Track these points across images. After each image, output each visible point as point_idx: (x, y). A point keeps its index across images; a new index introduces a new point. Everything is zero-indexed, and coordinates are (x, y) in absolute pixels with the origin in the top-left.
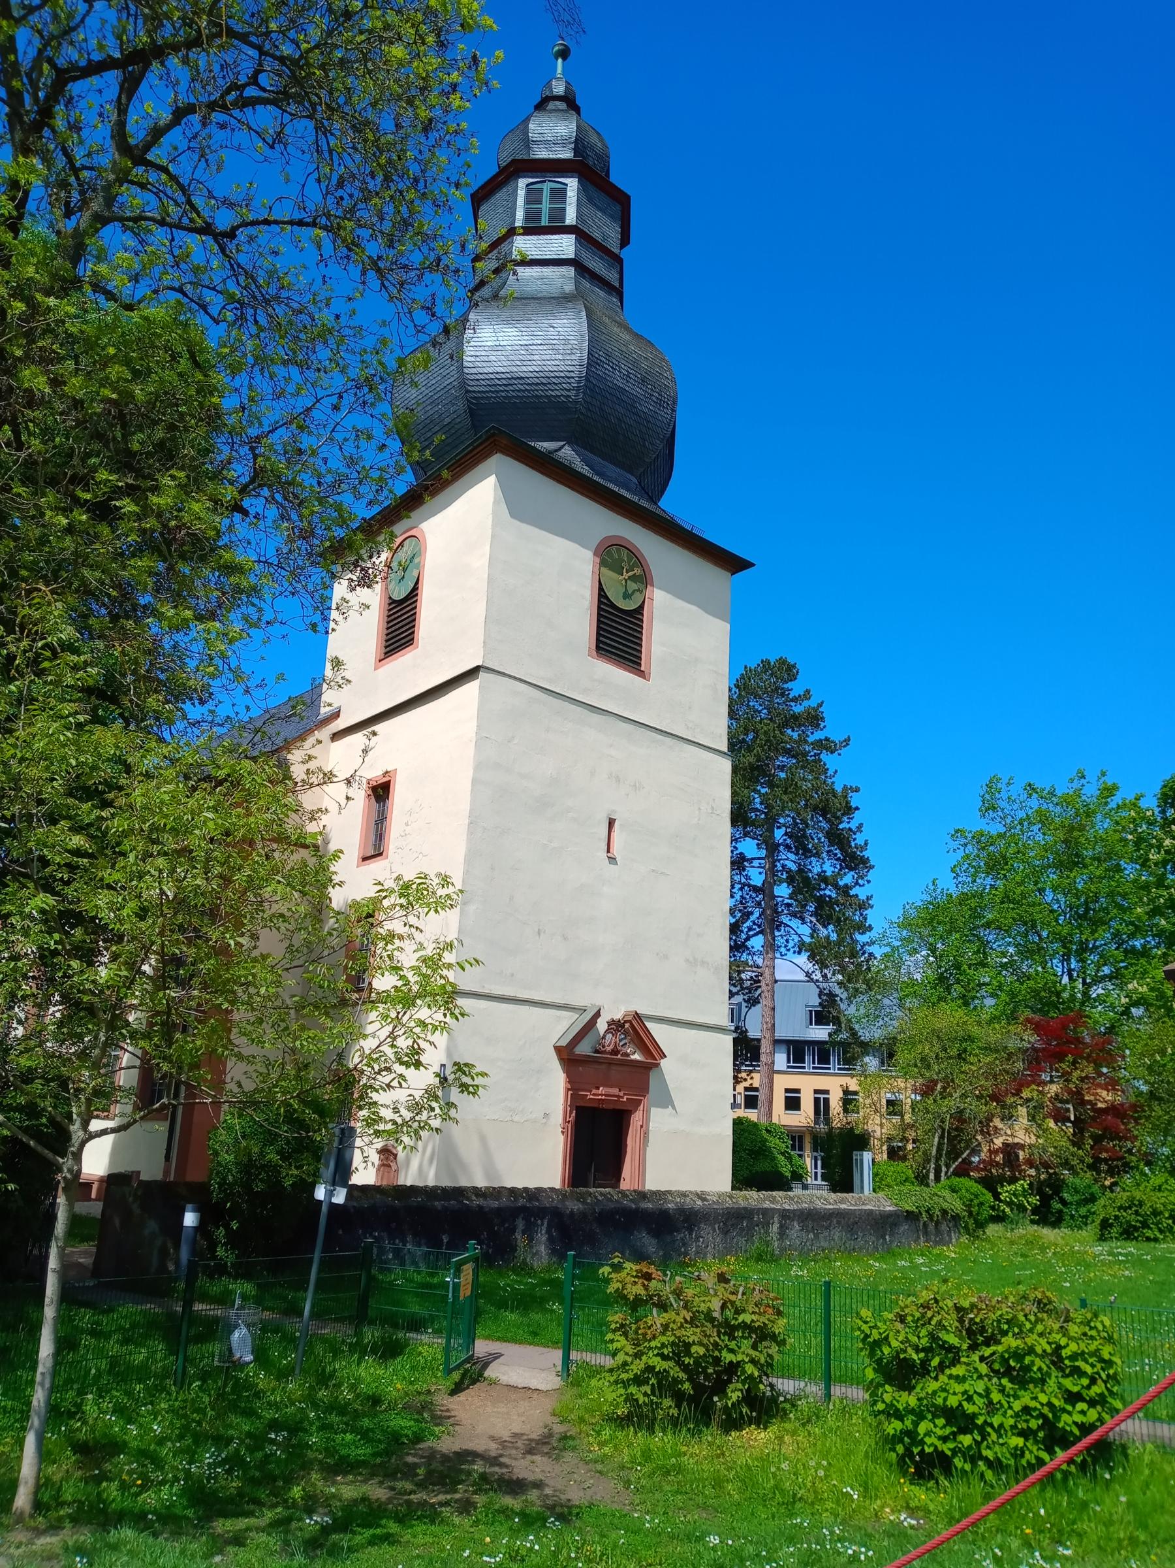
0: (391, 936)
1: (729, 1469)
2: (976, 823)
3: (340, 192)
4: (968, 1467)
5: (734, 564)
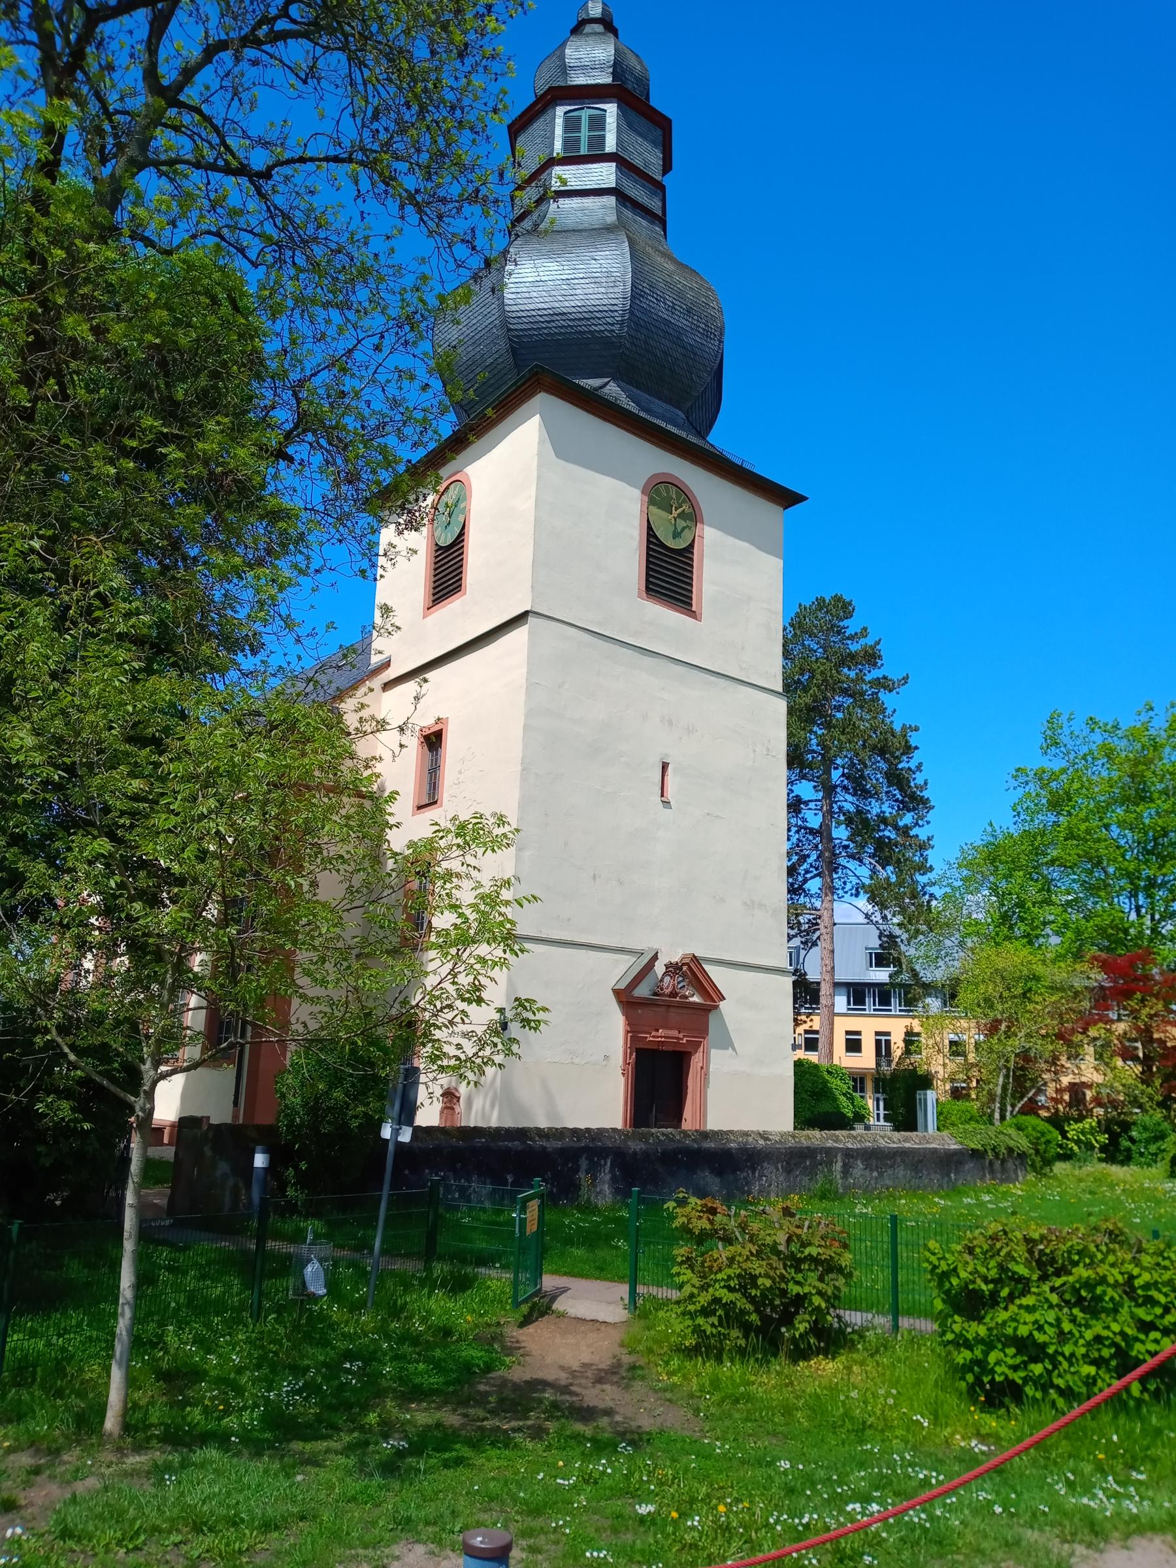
0: (449, 875)
1: (798, 1398)
2: (1036, 761)
3: (375, 125)
4: (1039, 1395)
5: (787, 498)
